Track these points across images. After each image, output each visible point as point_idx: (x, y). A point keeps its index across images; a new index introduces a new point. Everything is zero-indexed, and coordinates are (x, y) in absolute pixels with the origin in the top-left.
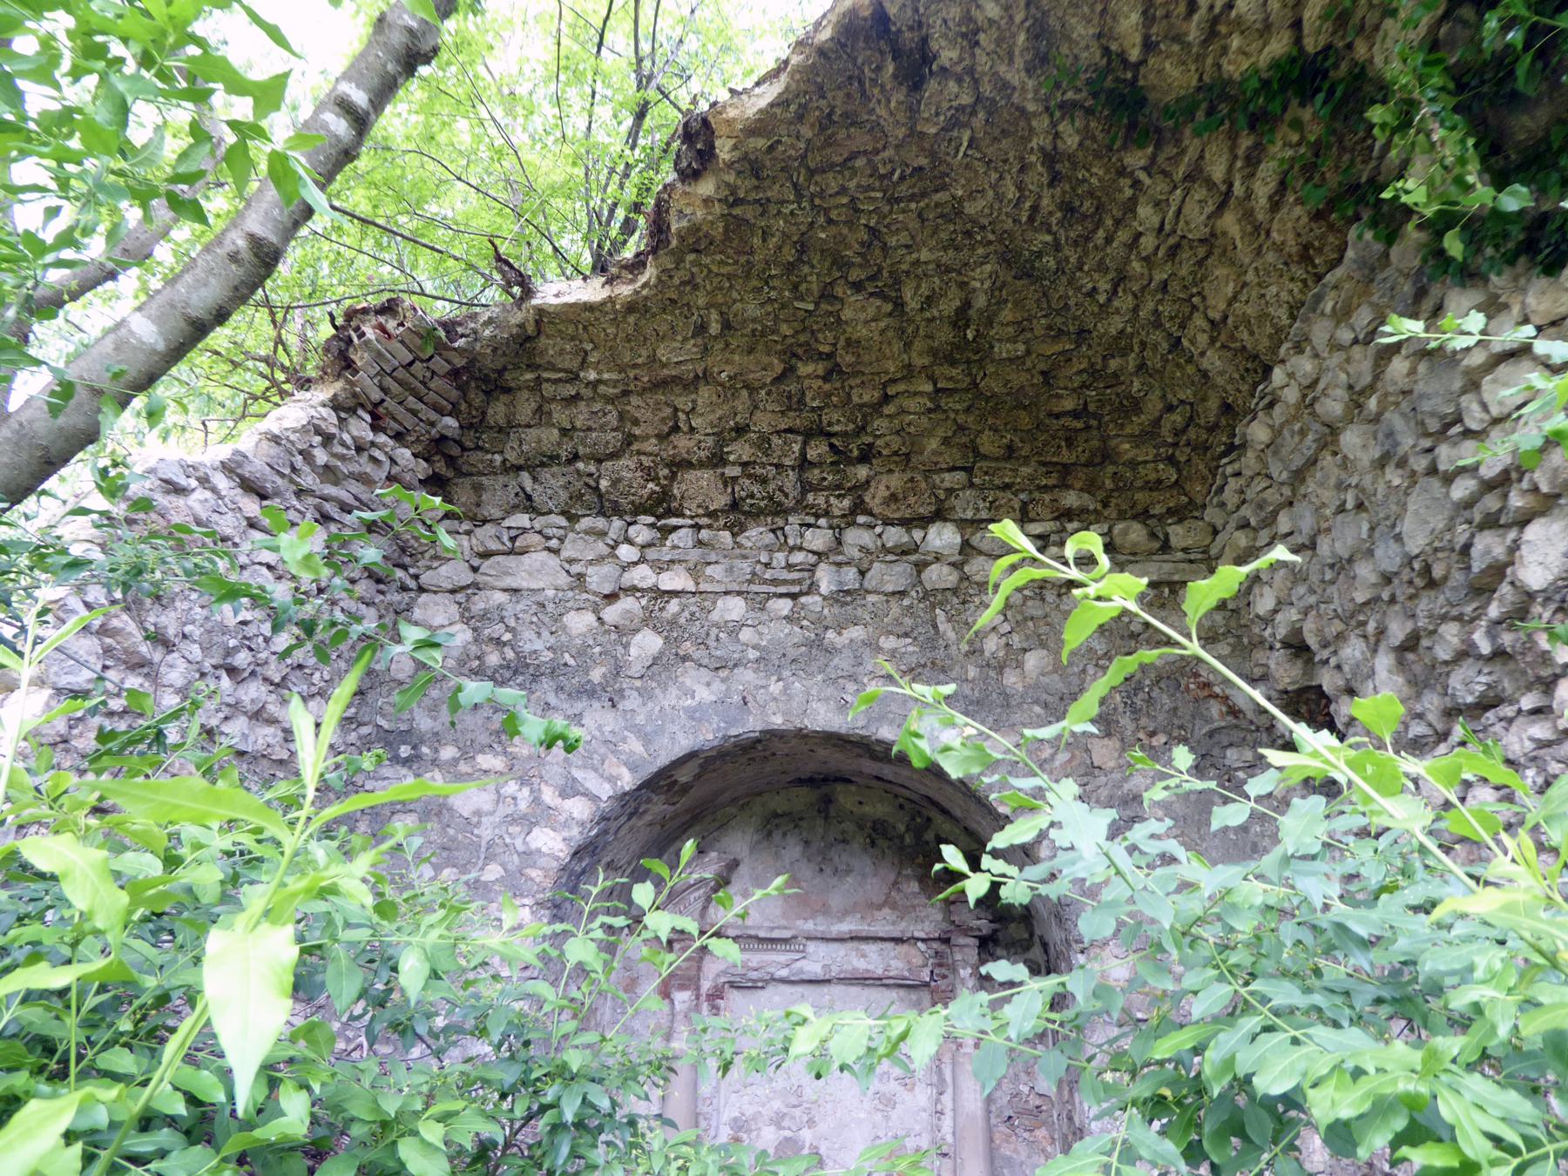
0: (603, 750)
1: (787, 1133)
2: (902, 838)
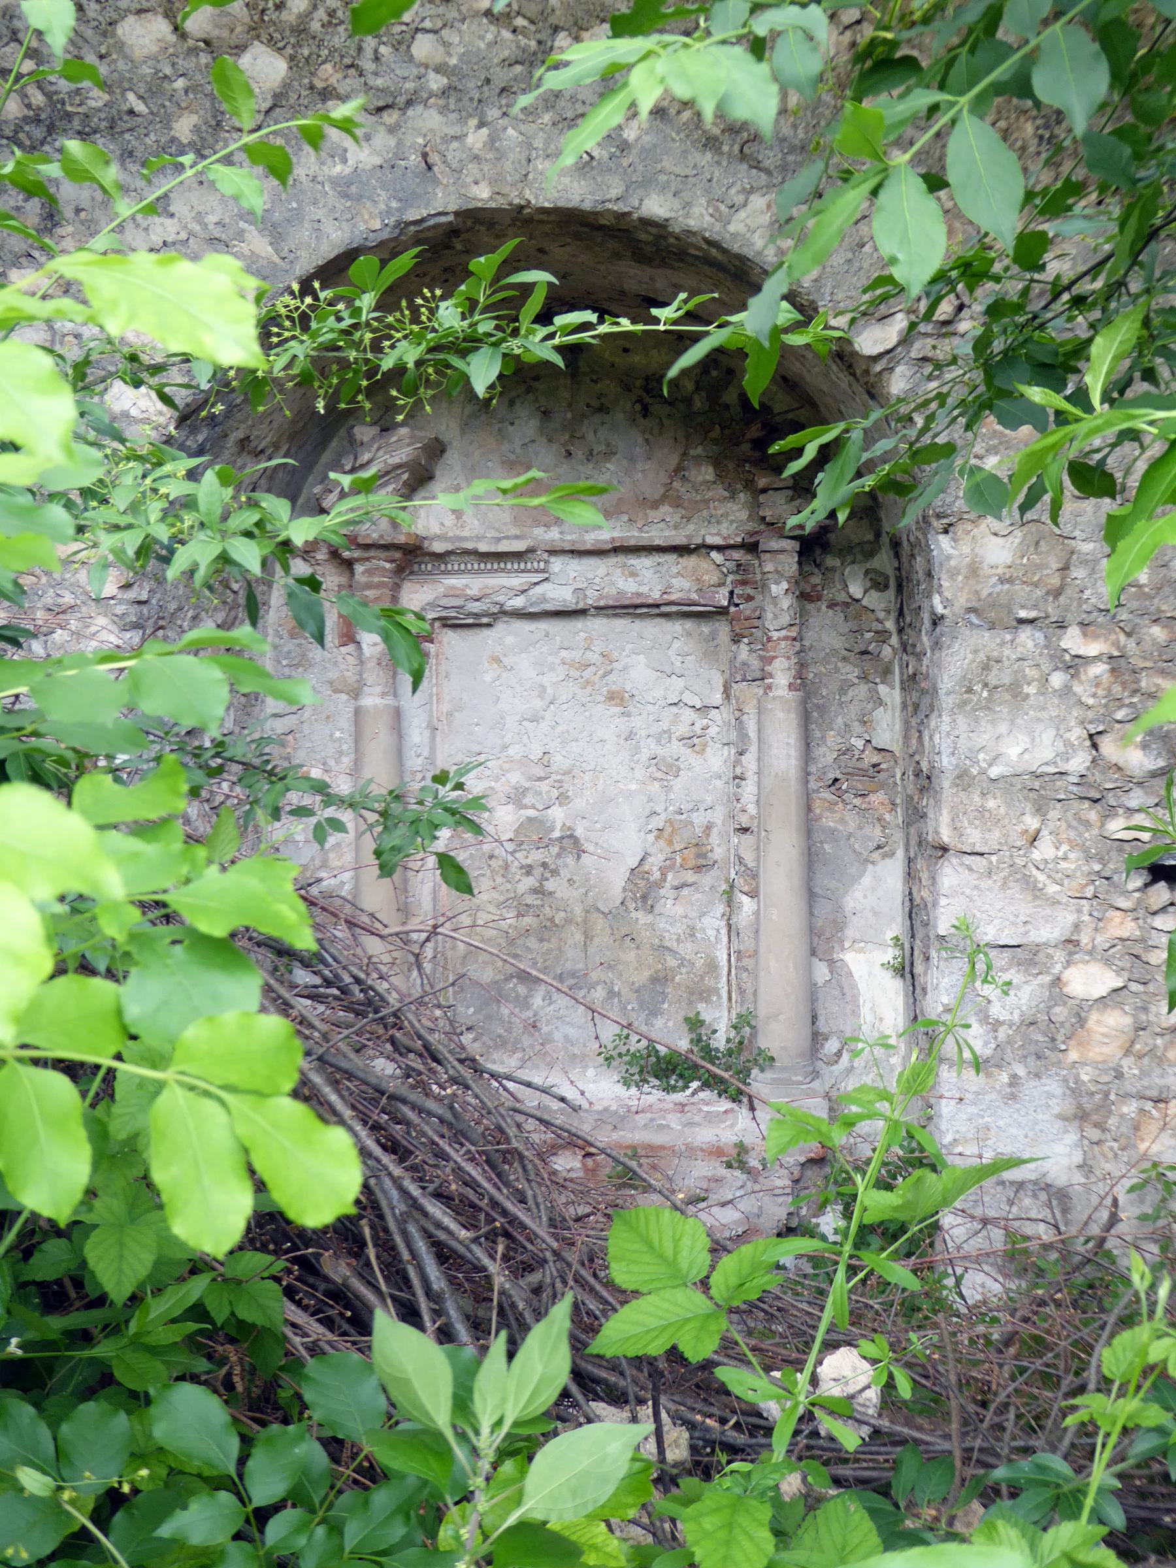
1: (531, 813)
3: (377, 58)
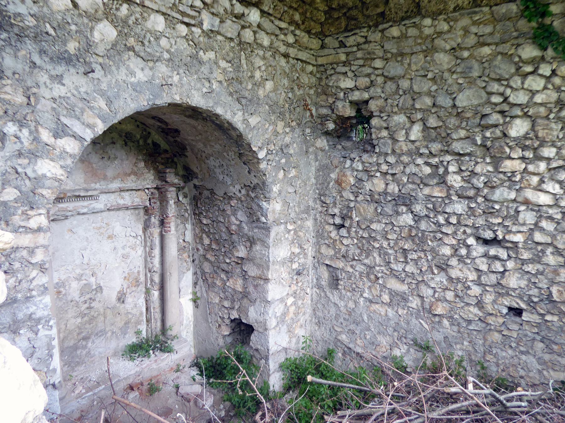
0: (80, 105)
1: (85, 282)
2: (138, 141)
3: (149, 42)
